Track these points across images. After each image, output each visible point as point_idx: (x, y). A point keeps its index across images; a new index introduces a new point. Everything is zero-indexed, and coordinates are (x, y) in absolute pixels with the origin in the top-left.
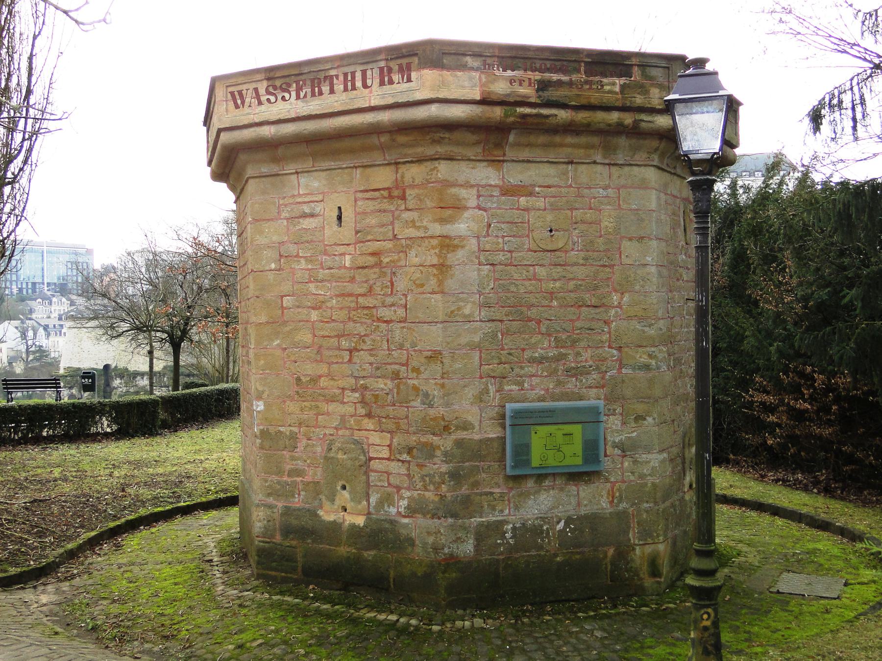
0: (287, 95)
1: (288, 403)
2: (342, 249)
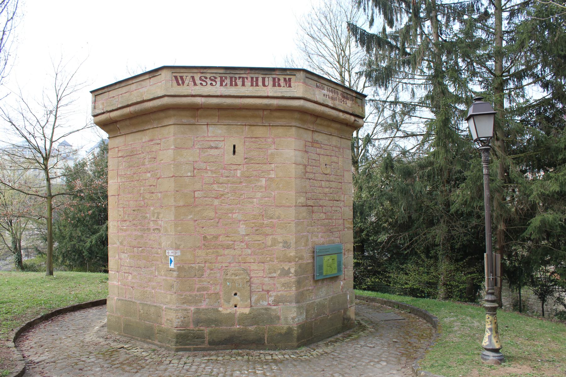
0: (214, 83)
1: (197, 251)
2: (235, 167)
